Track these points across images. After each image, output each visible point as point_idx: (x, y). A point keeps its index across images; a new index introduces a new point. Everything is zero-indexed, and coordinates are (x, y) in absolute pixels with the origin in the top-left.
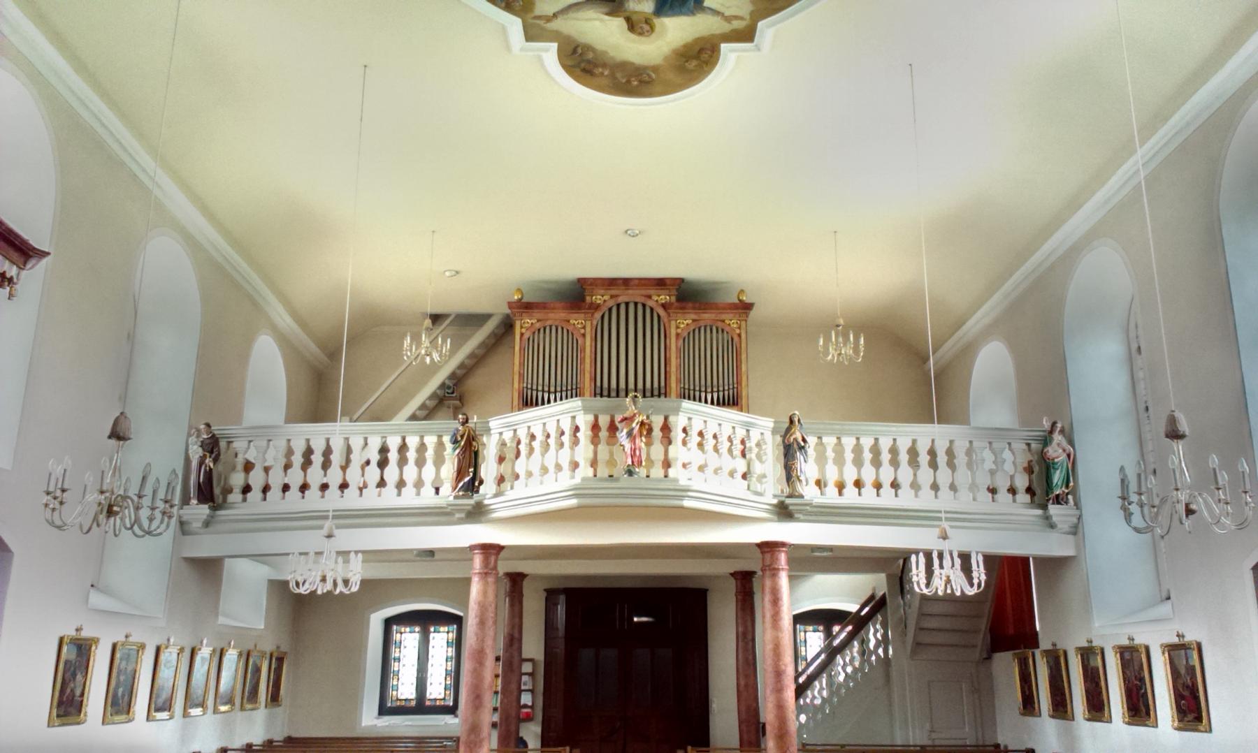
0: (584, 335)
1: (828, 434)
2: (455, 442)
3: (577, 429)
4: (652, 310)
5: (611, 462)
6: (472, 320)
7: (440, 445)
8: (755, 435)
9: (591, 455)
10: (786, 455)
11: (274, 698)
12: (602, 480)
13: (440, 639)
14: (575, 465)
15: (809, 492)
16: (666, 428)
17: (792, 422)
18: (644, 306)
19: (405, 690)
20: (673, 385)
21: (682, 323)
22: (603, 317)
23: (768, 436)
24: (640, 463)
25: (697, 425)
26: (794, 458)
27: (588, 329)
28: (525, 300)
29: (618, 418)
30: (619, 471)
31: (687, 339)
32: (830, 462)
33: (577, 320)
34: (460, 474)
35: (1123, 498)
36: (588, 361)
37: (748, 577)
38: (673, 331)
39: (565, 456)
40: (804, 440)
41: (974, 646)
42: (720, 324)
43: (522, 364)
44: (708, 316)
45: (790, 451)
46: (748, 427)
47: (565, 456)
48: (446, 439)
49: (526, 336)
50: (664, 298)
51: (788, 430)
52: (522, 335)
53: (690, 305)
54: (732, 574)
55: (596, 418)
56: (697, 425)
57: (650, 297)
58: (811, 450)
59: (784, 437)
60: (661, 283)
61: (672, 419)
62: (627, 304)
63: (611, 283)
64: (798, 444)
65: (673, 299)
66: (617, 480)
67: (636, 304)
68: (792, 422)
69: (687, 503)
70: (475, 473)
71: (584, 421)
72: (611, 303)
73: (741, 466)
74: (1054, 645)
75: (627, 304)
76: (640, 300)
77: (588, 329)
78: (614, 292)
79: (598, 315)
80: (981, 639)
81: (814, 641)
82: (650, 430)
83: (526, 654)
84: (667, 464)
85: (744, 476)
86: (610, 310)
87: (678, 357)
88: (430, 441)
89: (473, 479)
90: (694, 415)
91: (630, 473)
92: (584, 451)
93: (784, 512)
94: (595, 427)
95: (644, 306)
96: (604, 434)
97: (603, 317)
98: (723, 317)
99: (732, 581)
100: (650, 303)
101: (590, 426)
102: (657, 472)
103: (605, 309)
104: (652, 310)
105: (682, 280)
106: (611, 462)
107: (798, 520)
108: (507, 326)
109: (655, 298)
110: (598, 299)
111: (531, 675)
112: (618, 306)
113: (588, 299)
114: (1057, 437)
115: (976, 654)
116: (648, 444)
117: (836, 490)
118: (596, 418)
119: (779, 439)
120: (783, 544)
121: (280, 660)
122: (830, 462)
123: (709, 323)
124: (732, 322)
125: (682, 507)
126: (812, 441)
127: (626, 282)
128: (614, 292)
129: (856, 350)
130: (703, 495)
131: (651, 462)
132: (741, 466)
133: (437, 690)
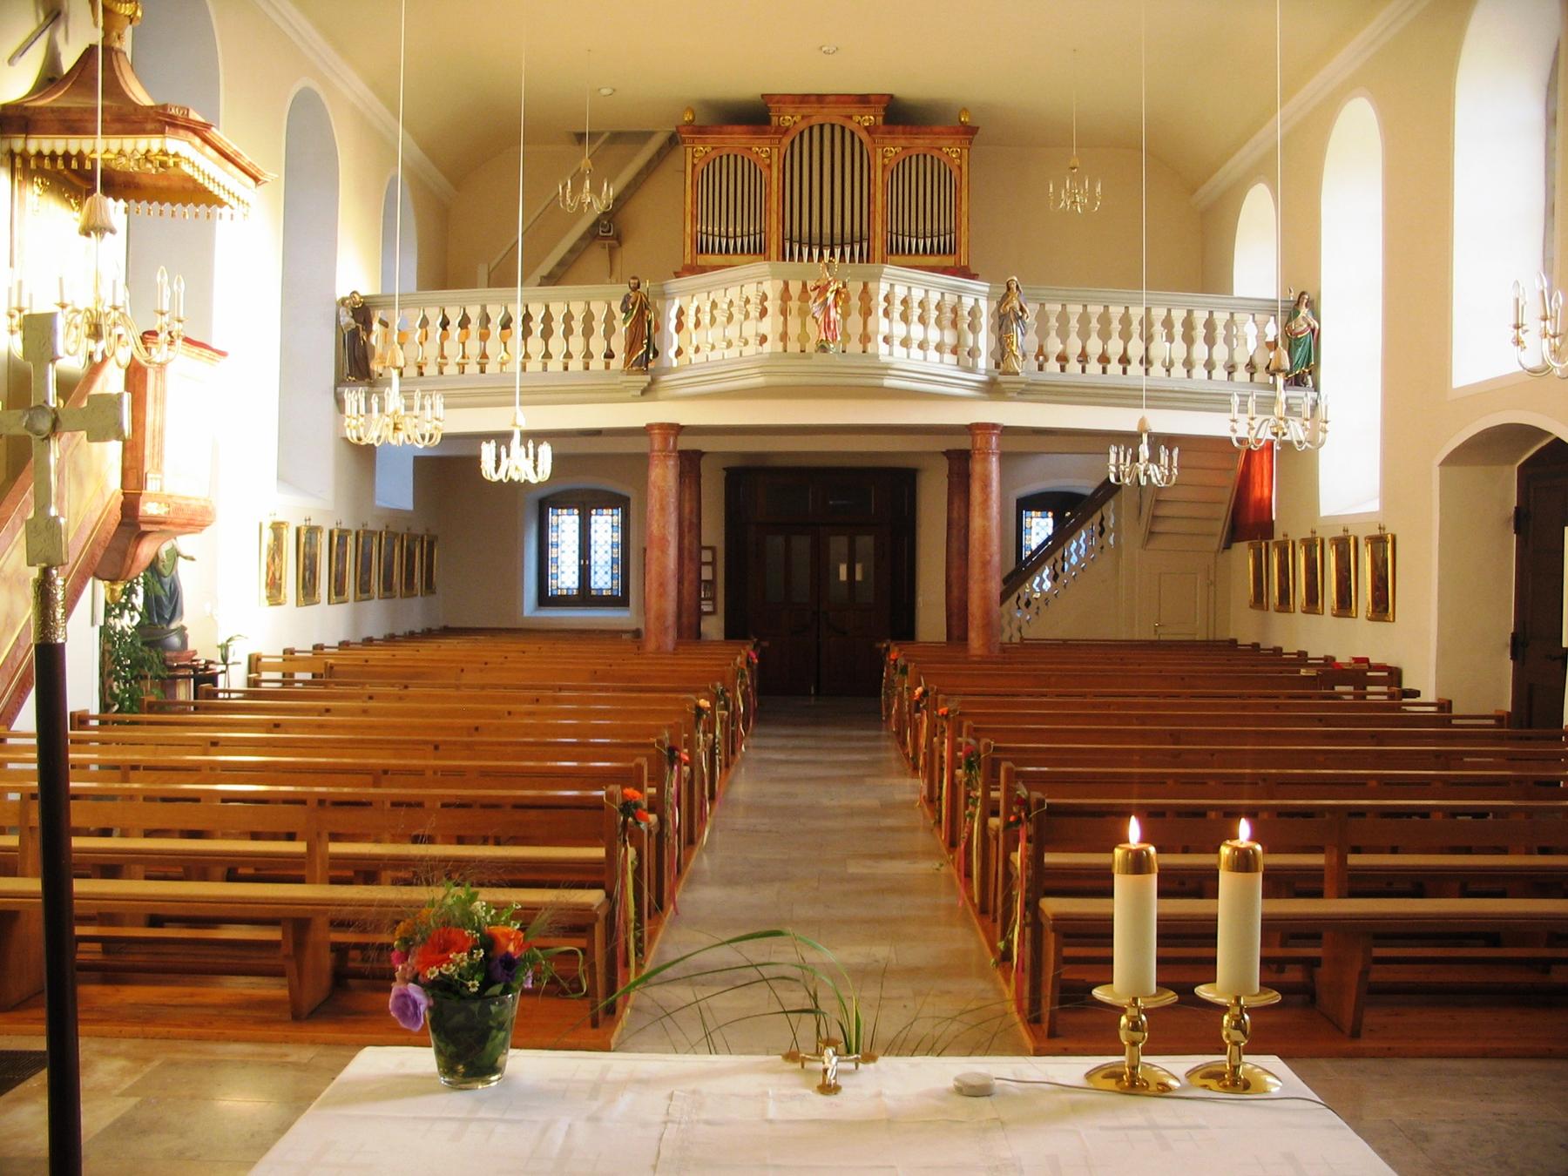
0: (770, 166)
1: (1050, 301)
2: (624, 309)
3: (764, 298)
4: (852, 134)
5: (803, 337)
6: (624, 137)
7: (610, 317)
8: (968, 302)
9: (780, 329)
10: (265, 1148)
11: (429, 586)
12: (794, 357)
13: (605, 526)
14: (763, 339)
15: (1025, 368)
16: (866, 296)
17: (1009, 289)
18: (843, 128)
19: (566, 578)
20: (879, 229)
21: (890, 150)
22: (792, 143)
23: (983, 304)
24: (834, 339)
25: (900, 292)
26: (1008, 330)
27: (775, 159)
28: (696, 123)
29: (811, 284)
30: (811, 347)
31: (895, 172)
32: (1053, 333)
33: (763, 149)
34: (631, 348)
35: (1517, 327)
36: (774, 198)
37: (960, 454)
38: (879, 162)
39: (750, 329)
40: (1022, 309)
41: (1214, 535)
42: (936, 153)
43: (695, 202)
44: (921, 143)
45: (1004, 321)
46: (959, 293)
47: (750, 329)
48: (616, 307)
49: (699, 169)
50: (869, 119)
51: (1005, 296)
52: (694, 166)
53: (900, 128)
54: (944, 453)
55: (786, 284)
56: (900, 292)
57: (850, 117)
58: (1030, 319)
59: (1000, 304)
60: (864, 100)
61: (871, 286)
62: (822, 126)
63: (804, 99)
64: (1016, 314)
65: (880, 119)
66: (810, 357)
67: (833, 126)
68: (1009, 289)
69: (888, 382)
70: (648, 345)
71: (772, 288)
72: (803, 125)
73: (949, 337)
74: (1346, 530)
75: (822, 126)
76: (838, 121)
77: (775, 159)
78: (806, 111)
79: (787, 141)
80: (1220, 527)
81: (1039, 528)
82: (847, 300)
83: (706, 540)
84: (865, 338)
85: (954, 351)
86: (801, 134)
87: (885, 192)
88: (599, 309)
89: (647, 352)
90: (898, 282)
91: (823, 348)
92: (770, 326)
93: (991, 390)
94: (785, 295)
95: (843, 128)
96: (794, 305)
97: (792, 143)
98: (941, 143)
99: (945, 463)
100: (850, 126)
101: (778, 295)
102: (854, 347)
103: (795, 133)
104: (852, 134)
105: (891, 96)
106: (803, 337)
107: (1011, 399)
108: (673, 141)
109: (857, 118)
110: (787, 120)
111: (713, 564)
112: (811, 129)
113: (774, 120)
114: (1304, 311)
115: (1216, 543)
116: (846, 315)
117: (1058, 365)
118: (786, 284)
119: (994, 305)
120: (994, 426)
121: (431, 545)
122: (1053, 333)
123: (921, 151)
124: (951, 150)
125: (882, 387)
126: (1031, 309)
127: (821, 98)
128: (806, 111)
129: (1092, 199)
130: (904, 374)
131: (847, 337)
132: (949, 337)
133: (603, 579)
